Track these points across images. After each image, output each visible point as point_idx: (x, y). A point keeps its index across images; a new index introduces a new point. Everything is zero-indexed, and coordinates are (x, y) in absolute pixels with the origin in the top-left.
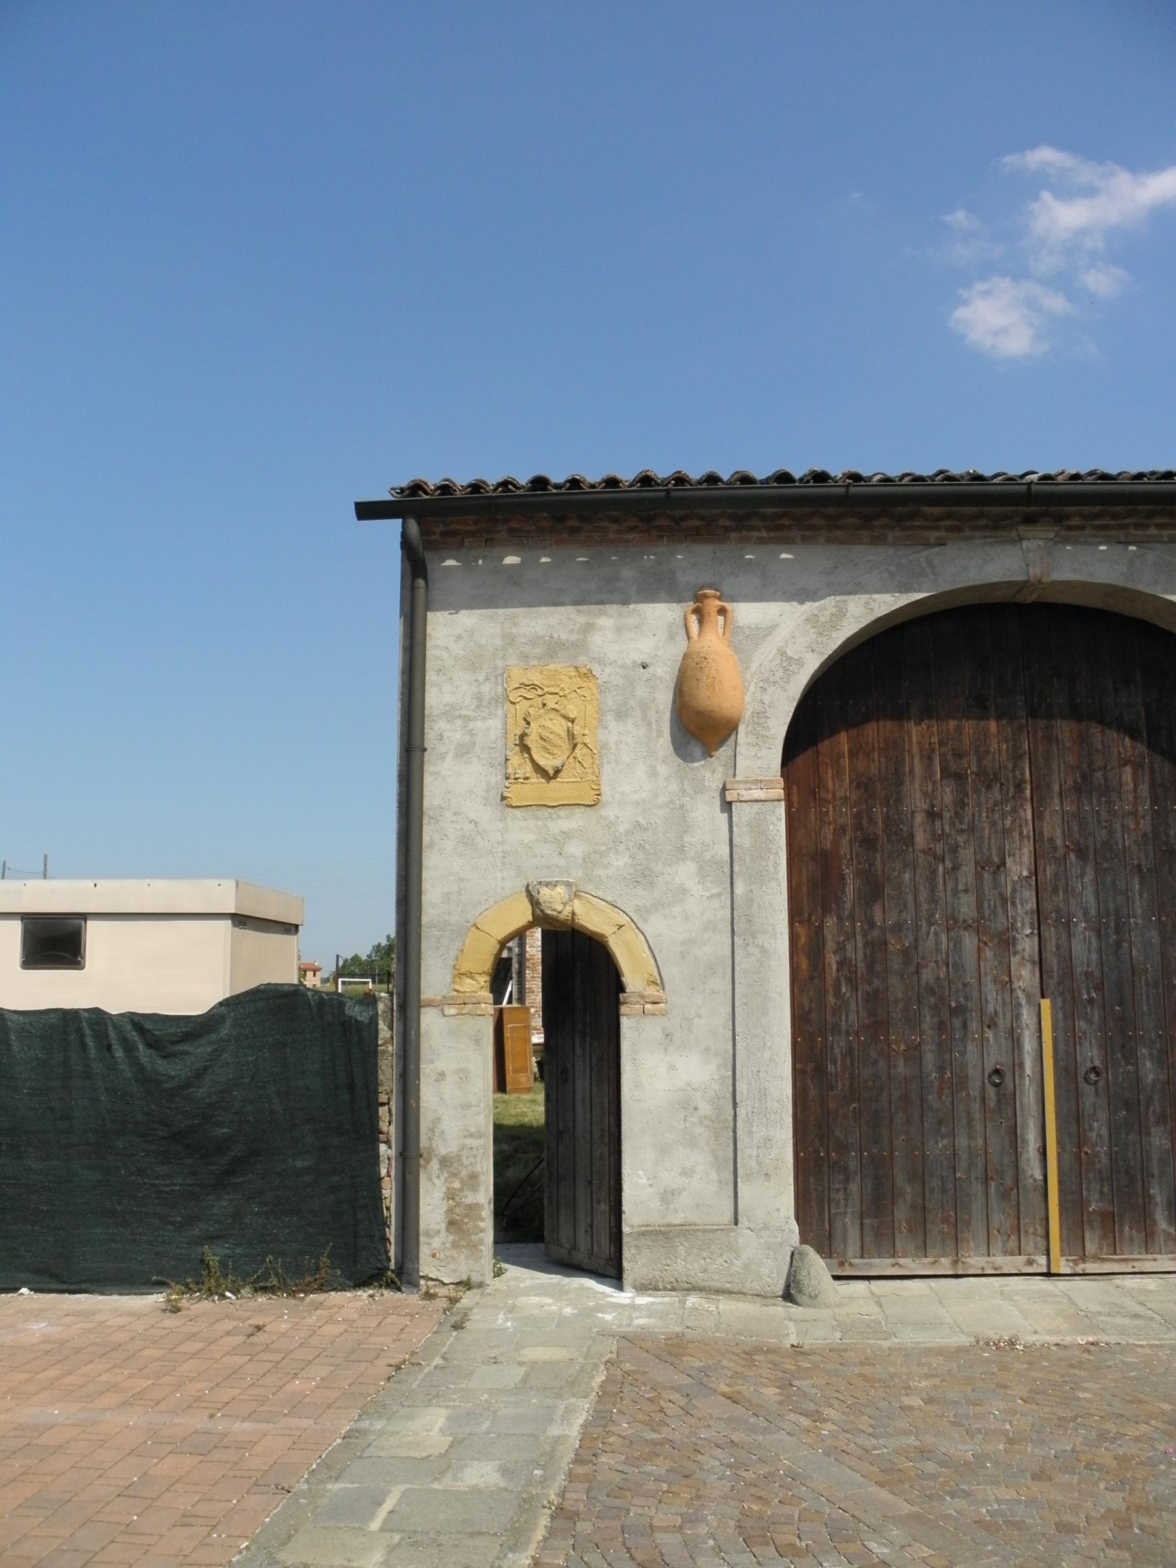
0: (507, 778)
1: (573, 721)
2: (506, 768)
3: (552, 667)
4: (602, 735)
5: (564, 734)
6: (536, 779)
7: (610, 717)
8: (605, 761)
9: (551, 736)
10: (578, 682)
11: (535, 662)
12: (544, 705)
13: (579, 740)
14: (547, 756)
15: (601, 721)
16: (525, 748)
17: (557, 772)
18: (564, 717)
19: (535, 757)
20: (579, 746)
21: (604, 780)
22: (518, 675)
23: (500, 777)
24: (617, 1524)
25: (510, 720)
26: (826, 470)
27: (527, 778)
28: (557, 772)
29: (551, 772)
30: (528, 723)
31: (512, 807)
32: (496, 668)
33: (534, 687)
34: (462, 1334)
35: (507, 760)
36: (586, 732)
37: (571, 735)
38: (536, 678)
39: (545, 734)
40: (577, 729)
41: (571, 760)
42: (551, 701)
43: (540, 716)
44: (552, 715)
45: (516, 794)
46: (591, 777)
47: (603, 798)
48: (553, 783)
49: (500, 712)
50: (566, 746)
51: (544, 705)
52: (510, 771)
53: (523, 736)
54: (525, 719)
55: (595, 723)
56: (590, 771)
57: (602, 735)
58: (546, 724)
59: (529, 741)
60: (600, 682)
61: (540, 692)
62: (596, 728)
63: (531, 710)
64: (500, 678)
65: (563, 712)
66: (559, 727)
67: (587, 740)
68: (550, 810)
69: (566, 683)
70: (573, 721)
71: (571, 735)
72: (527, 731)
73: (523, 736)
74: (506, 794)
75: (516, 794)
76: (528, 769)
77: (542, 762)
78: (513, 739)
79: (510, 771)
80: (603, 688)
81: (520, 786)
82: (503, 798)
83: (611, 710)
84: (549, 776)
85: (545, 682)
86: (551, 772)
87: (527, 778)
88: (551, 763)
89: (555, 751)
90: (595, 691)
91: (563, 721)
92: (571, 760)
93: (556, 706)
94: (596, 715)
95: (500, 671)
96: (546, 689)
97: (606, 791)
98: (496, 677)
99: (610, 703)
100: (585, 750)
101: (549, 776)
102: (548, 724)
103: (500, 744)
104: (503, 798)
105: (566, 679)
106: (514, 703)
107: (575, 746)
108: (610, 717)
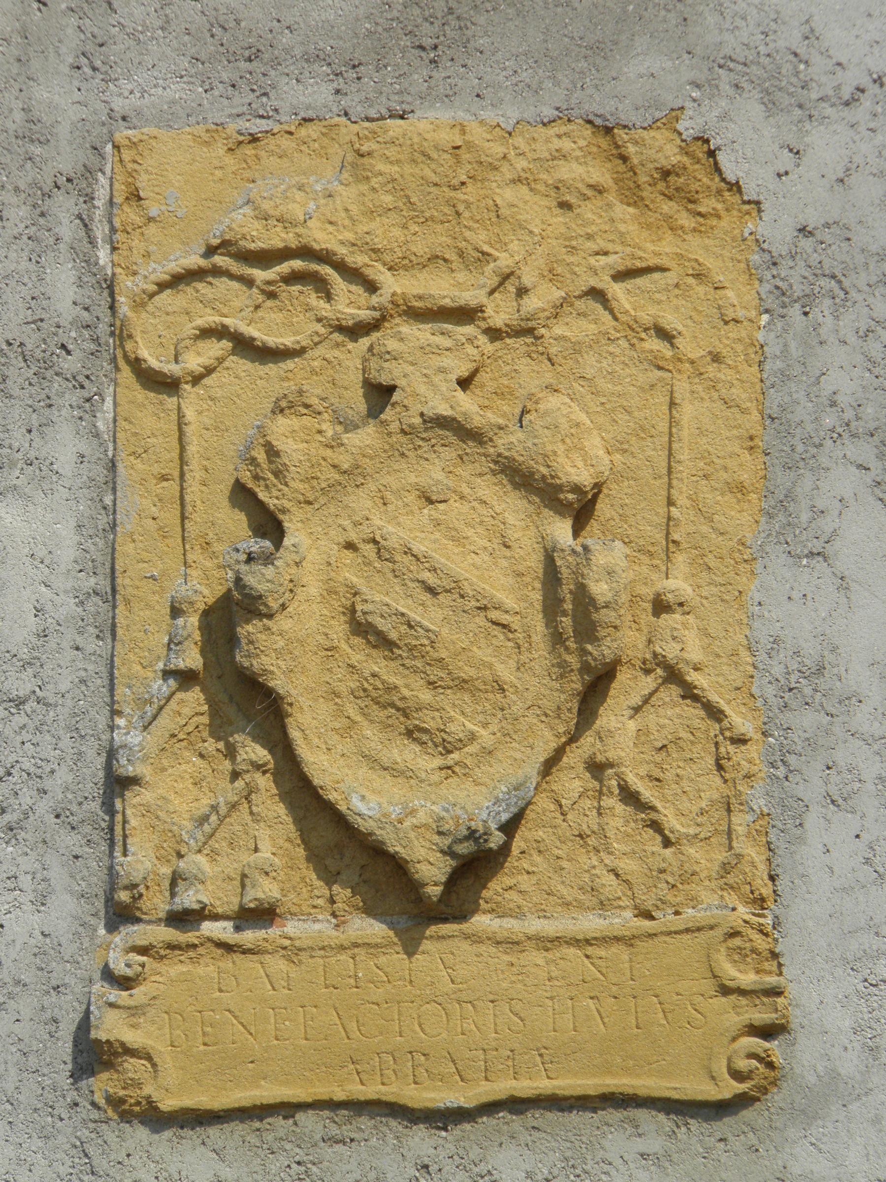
0: (120, 915)
1: (582, 510)
2: (114, 838)
3: (432, 123)
4: (790, 607)
5: (521, 601)
6: (323, 921)
7: (843, 481)
8: (811, 786)
9: (431, 616)
10: (623, 231)
11: (317, 93)
12: (380, 394)
13: (625, 639)
14: (405, 753)
15: (779, 506)
16: (247, 703)
17: (476, 864)
18: (521, 478)
19: (322, 764)
20: (628, 687)
21: (810, 919)
22: (192, 190)
23: (68, 911)
24: (846, 1139)
25: (141, 503)
26: (226, 503)
27: (261, 915)
28: (476, 864)
29: (432, 871)
30: (269, 526)
31: (156, 1119)
32: (34, 132)
33: (309, 267)
34: (801, 220)
35: (117, 784)
36: (678, 584)
37: (569, 607)
38: (313, 202)
39: (385, 599)
40: (610, 566)
41: (572, 782)
42: (427, 369)
43: (353, 475)
44: (437, 467)
45: (189, 1024)
46: (710, 904)
47: (803, 1057)
48: (445, 952)
49: (66, 446)
50: (535, 680)
51: (380, 394)
52: (141, 860)
53: (231, 614)
54: (242, 495)
55: (740, 519)
56: (705, 858)
57: (790, 607)
58: (395, 533)
59: (276, 652)
60: (776, 228)
61: (349, 303)
62: (748, 559)
63: (285, 431)
64: (64, 207)
65: (512, 442)
66: (487, 544)
67: (683, 640)
68: (422, 1141)
69: (532, 237)
70: (582, 510)
71: (569, 607)
72: (258, 579)
73: (231, 614)
74: (111, 1027)
75: (189, 1024)
76: (268, 848)
77: (368, 800)
78: (156, 640)
79: (141, 860)
80: (795, 276)
81: (207, 968)
82: (93, 1056)
83: (847, 430)
84: (420, 895)
85: (386, 232)
86: (432, 871)
87: (261, 915)
88: (427, 809)
89: (460, 718)
90: (739, 296)
91: (513, 509)
92: (572, 782)
93: (466, 406)
94: (747, 468)
95: (66, 159)
96: (392, 285)
97: (823, 1004)
98: (40, 198)
99: (844, 380)
100: (672, 715)
101: (420, 895)
102: (406, 528)
103: (67, 672)
104: (93, 1056)
105: (534, 210)
106: (167, 385)
107: (597, 684)
108: (843, 481)
